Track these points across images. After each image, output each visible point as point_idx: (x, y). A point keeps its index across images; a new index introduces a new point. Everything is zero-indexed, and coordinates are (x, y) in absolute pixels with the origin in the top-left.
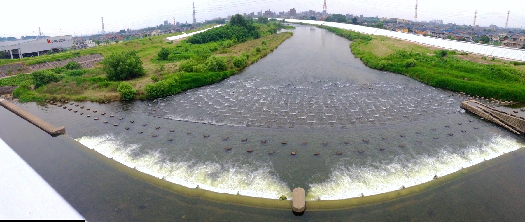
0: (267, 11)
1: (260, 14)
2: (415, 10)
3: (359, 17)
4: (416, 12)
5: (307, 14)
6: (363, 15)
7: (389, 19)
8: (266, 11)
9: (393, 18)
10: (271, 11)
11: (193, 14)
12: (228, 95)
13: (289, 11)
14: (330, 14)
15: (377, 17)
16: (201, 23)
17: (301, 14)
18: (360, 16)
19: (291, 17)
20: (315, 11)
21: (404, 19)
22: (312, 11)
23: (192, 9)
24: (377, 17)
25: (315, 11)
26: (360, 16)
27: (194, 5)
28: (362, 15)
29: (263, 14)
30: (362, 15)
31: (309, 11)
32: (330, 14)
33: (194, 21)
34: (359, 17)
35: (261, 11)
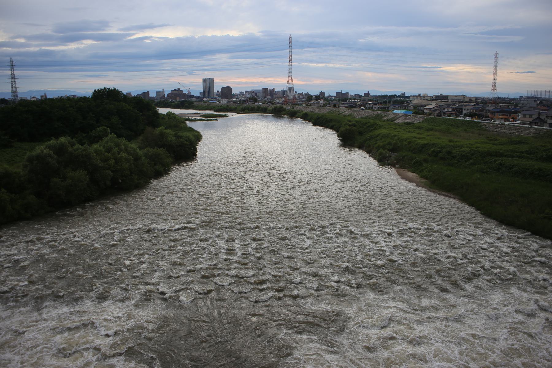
0: (175, 90)
1: (162, 95)
2: (491, 77)
3: (363, 95)
4: (495, 79)
5: (256, 94)
6: (370, 93)
7: (433, 97)
8: (172, 91)
9: (441, 95)
10: (182, 91)
11: (12, 82)
12: (241, 245)
13: (220, 90)
14: (303, 92)
15: (404, 94)
16: (32, 99)
17: (243, 95)
18: (365, 94)
19: (224, 100)
20: (273, 90)
21: (464, 95)
22: (267, 89)
23: (10, 85)
24: (404, 94)
25: (273, 90)
26: (365, 94)
27: (14, 64)
28: (368, 92)
29: (168, 95)
30: (368, 92)
31: (262, 89)
32: (303, 92)
33: (13, 96)
34: (363, 95)
35: (163, 90)
